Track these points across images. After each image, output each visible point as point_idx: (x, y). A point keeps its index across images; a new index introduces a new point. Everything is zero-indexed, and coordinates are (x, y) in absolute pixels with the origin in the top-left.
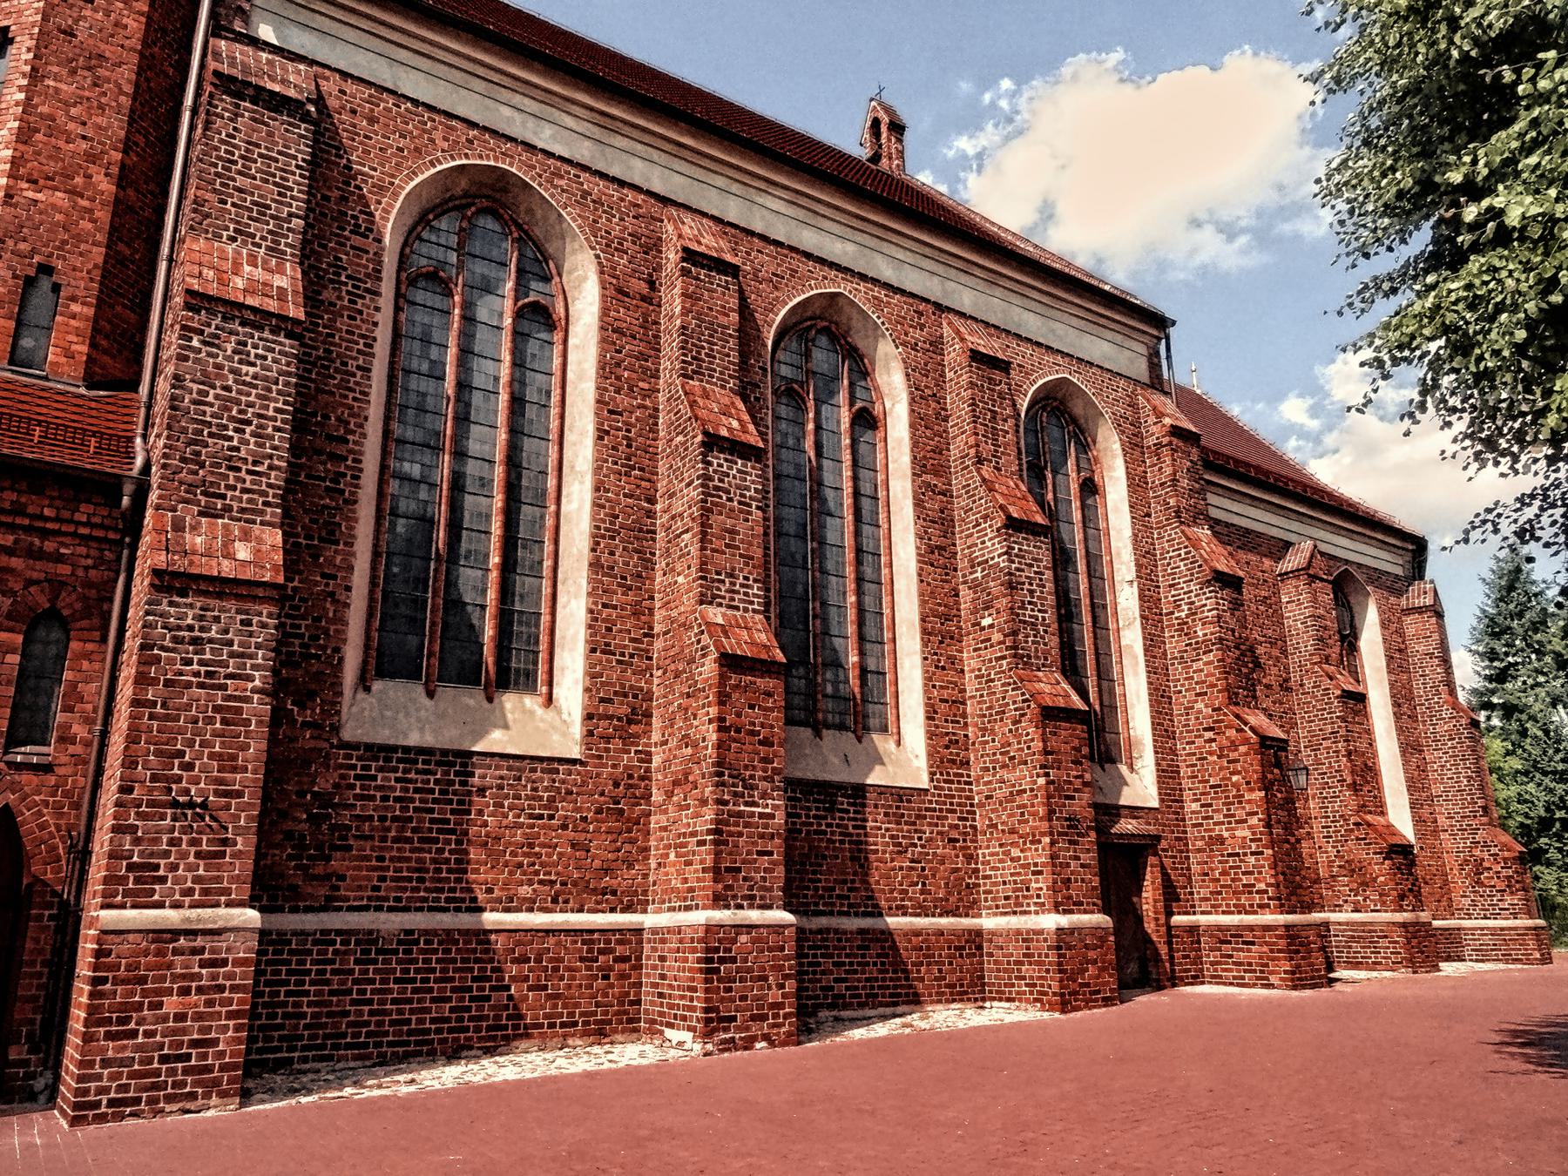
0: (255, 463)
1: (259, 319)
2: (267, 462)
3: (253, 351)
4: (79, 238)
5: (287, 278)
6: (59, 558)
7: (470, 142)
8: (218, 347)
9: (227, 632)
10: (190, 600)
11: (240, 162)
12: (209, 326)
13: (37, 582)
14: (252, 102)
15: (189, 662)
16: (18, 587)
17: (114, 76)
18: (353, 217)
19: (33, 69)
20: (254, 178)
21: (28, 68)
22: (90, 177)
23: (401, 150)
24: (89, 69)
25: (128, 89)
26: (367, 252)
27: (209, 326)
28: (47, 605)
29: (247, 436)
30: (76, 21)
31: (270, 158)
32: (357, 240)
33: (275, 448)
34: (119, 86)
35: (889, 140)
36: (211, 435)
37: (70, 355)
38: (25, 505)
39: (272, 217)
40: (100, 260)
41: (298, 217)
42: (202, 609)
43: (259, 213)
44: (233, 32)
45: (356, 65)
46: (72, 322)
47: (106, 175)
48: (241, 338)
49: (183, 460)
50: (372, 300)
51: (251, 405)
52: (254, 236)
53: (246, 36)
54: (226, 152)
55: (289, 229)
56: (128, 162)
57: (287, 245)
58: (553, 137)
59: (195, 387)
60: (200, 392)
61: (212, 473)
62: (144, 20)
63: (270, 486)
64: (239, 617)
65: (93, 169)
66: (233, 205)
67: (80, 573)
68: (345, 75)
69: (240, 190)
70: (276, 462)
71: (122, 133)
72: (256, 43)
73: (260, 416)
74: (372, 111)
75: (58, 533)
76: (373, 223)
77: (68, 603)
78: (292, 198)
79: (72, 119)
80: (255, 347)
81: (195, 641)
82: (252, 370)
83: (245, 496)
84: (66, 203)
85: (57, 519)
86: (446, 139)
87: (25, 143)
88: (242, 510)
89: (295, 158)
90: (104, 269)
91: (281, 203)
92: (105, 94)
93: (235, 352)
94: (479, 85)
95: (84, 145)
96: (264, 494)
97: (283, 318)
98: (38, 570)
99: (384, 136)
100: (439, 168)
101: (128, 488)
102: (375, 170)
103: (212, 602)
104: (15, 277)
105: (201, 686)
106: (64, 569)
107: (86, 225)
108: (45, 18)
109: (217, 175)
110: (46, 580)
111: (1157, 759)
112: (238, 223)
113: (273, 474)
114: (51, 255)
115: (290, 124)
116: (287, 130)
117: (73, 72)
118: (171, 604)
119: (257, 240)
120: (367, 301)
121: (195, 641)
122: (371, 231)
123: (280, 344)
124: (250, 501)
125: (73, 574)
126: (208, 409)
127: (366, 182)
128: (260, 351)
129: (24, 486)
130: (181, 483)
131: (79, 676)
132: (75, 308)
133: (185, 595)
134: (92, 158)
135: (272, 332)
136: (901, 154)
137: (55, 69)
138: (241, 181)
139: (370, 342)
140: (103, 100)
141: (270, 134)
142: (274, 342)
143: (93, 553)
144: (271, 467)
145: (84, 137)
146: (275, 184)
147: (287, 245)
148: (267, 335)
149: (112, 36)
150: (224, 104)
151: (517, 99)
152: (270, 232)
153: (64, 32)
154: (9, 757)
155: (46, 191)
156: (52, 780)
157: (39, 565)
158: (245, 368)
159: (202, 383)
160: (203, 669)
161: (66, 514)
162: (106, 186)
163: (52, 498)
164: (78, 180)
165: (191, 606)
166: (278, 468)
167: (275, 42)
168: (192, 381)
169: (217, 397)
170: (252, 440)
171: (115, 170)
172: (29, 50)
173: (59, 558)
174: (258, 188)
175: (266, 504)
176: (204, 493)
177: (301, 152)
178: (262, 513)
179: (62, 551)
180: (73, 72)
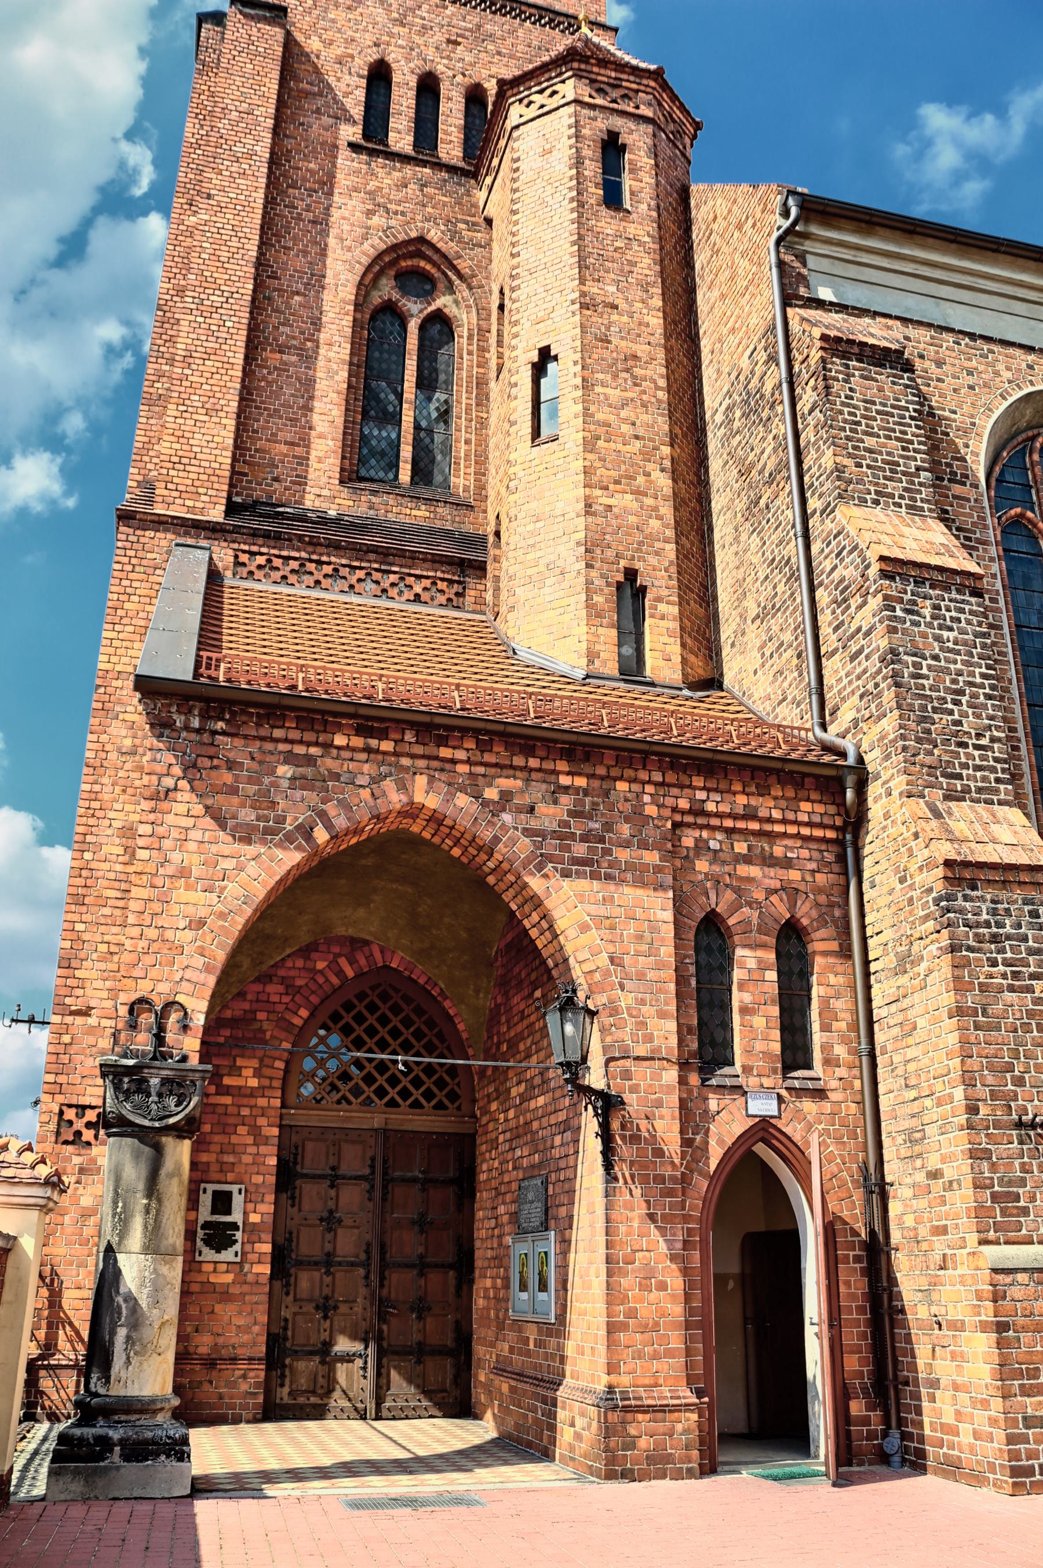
0: (979, 736)
2: (988, 734)
3: (948, 614)
7: (1031, 367)
8: (919, 614)
9: (1019, 926)
10: (979, 893)
11: (863, 422)
12: (906, 592)
13: (776, 891)
14: (858, 360)
15: (994, 963)
16: (760, 896)
17: (649, 373)
18: (948, 465)
19: (584, 380)
20: (879, 436)
21: (578, 381)
22: (648, 475)
23: (971, 388)
24: (627, 370)
25: (662, 383)
26: (968, 500)
27: (906, 592)
28: (788, 916)
29: (965, 707)
30: (608, 329)
31: (887, 414)
32: (957, 489)
33: (991, 718)
34: (654, 382)
36: (935, 710)
38: (756, 809)
39: (904, 474)
40: (672, 556)
41: (925, 470)
42: (993, 902)
43: (892, 471)
44: (802, 298)
45: (908, 309)
46: (662, 623)
47: (662, 470)
48: (934, 601)
49: (919, 740)
50: (985, 550)
51: (959, 673)
52: (892, 496)
53: (809, 299)
54: (850, 414)
55: (921, 484)
56: (676, 455)
57: (922, 500)
59: (910, 659)
60: (915, 665)
61: (946, 751)
62: (661, 315)
63: (997, 760)
64: (1027, 908)
65: (649, 466)
66: (869, 467)
67: (809, 878)
69: (871, 451)
70: (995, 733)
71: (666, 427)
72: (820, 304)
73: (971, 684)
74: (937, 352)
75: (785, 835)
76: (966, 468)
78: (915, 451)
79: (624, 421)
80: (948, 610)
81: (995, 939)
82: (952, 635)
83: (979, 774)
84: (635, 505)
85: (784, 821)
86: (1008, 369)
87: (591, 452)
88: (979, 790)
89: (907, 409)
90: (678, 565)
91: (908, 458)
92: (644, 392)
93: (934, 617)
95: (638, 444)
96: (993, 770)
99: (954, 377)
100: (1011, 400)
101: (850, 780)
102: (955, 412)
103: (1003, 895)
104: (608, 584)
105: (1012, 989)
106: (794, 875)
107: (655, 523)
108: (583, 331)
109: (848, 438)
110: (783, 889)
112: (877, 484)
113: (996, 746)
114: (633, 558)
115: (894, 376)
116: (893, 383)
117: (615, 376)
118: (966, 898)
119: (897, 500)
120: (981, 553)
121: (995, 939)
122: (967, 477)
123: (968, 603)
124: (984, 779)
125: (803, 880)
126: (925, 682)
127: (950, 426)
128: (954, 614)
129: (753, 789)
130: (922, 765)
131: (831, 992)
132: (662, 607)
133: (974, 888)
135: (959, 592)
137: (600, 376)
138: (870, 442)
140: (644, 397)
141: (881, 390)
142: (963, 602)
143: (816, 855)
144: (993, 740)
145: (637, 437)
146: (897, 439)
147: (922, 500)
148: (954, 595)
149: (639, 336)
150: (836, 365)
152: (905, 489)
153: (602, 341)
154: (789, 1083)
155: (616, 495)
156: (827, 1107)
157: (772, 872)
158: (945, 634)
159: (915, 655)
160: (1008, 969)
161: (790, 816)
162: (664, 482)
163: (775, 798)
164: (641, 479)
165: (982, 899)
166: (998, 740)
167: (835, 300)
168: (906, 653)
169: (930, 668)
170: (970, 711)
171: (667, 463)
172: (575, 363)
173: (787, 863)
174: (884, 446)
175: (998, 780)
176: (945, 775)
178: (997, 791)
179: (789, 855)
180: (615, 376)
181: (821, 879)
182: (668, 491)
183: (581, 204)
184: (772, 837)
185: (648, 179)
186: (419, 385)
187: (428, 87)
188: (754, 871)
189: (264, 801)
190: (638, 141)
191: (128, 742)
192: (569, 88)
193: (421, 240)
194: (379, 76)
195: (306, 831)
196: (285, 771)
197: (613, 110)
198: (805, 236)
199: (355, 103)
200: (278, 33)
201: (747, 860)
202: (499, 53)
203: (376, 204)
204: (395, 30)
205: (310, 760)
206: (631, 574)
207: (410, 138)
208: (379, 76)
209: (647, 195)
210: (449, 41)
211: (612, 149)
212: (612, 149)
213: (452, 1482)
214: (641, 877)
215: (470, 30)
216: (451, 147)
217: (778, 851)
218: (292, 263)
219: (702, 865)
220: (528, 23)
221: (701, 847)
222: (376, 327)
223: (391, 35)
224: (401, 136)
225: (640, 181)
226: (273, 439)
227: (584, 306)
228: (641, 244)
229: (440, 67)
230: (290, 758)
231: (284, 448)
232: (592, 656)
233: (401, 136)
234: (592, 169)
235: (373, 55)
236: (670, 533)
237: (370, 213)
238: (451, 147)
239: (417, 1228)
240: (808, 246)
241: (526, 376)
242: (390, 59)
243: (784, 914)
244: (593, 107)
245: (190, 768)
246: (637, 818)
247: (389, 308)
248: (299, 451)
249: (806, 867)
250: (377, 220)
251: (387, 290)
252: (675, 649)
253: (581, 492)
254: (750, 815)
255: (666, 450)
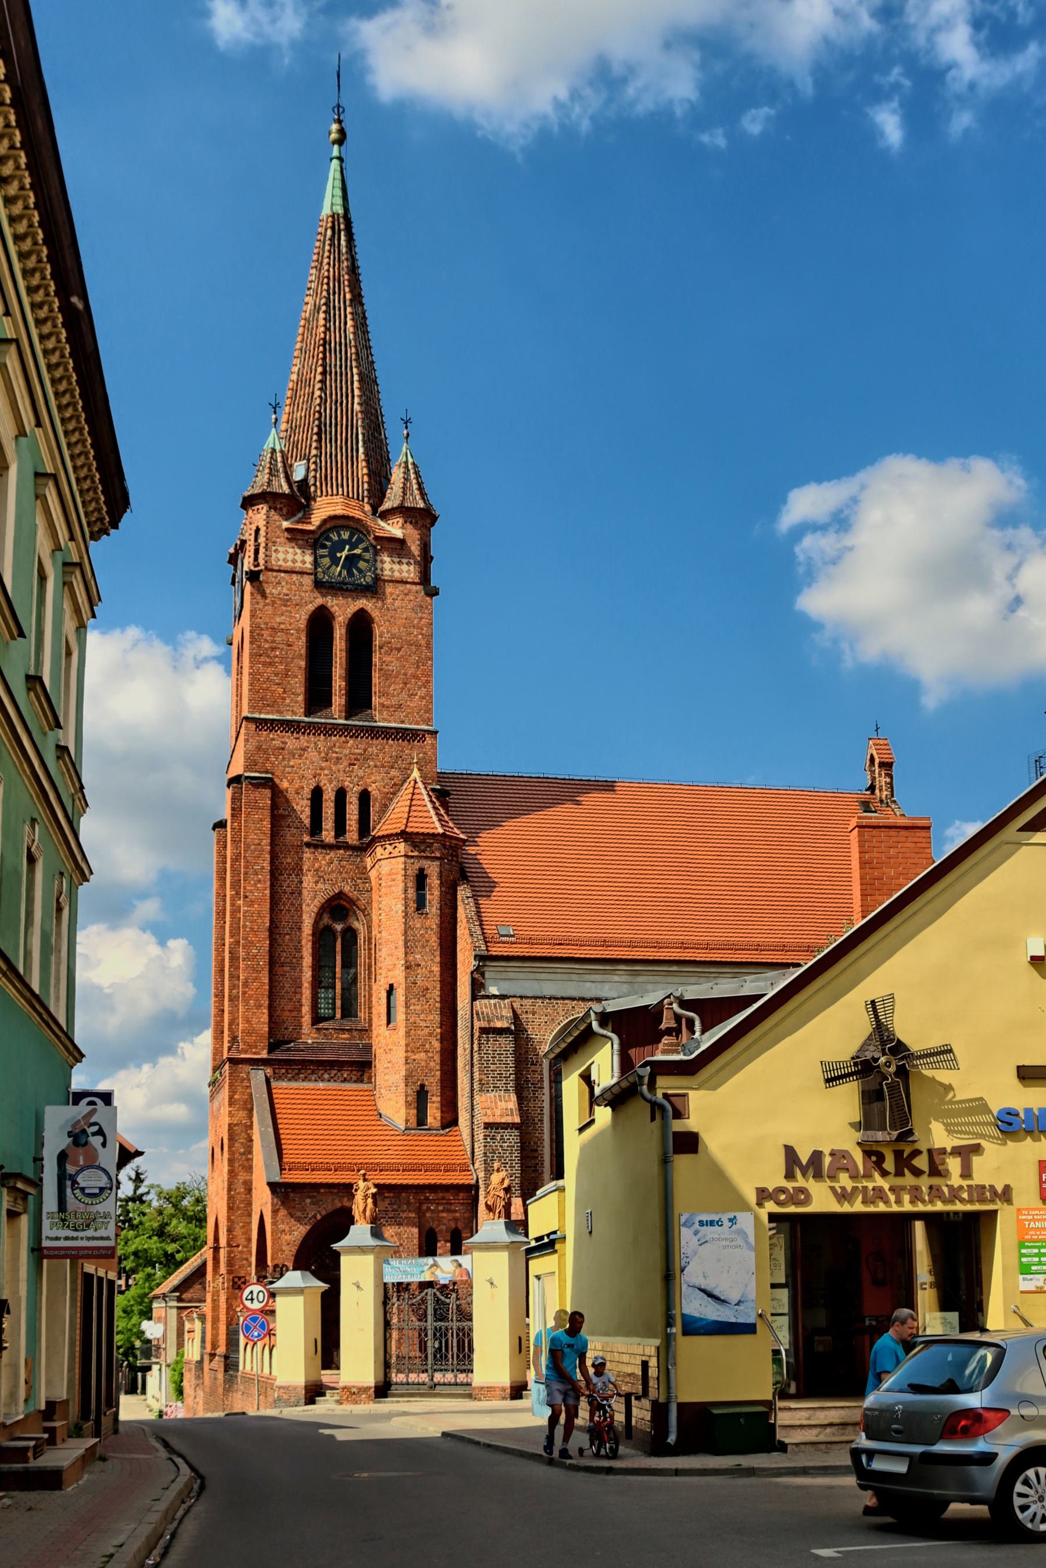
1: (505, 1126)
4: (431, 1070)
5: (511, 1102)
6: (456, 1211)
25: (438, 999)
32: (533, 1068)
35: (880, 775)
37: (435, 1118)
58: (610, 990)
68: (521, 997)
77: (460, 1225)
94: (574, 977)
97: (513, 1124)
98: (451, 1216)
106: (458, 1215)
107: (432, 1064)
111: (471, 1365)
134: (430, 1035)
136: (891, 785)
139: (542, 1108)
151: (593, 977)
162: (437, 1045)
164: (427, 1046)
171: (439, 1037)
173: (456, 1211)
177: (511, 1047)
181: (466, 1215)
182: (438, 1049)
183: (406, 915)
184: (451, 1204)
185: (437, 893)
186: (343, 966)
187: (341, 795)
188: (444, 1215)
189: (303, 1210)
190: (433, 869)
191: (242, 1150)
192: (402, 847)
193: (341, 893)
194: (317, 794)
195: (315, 1216)
196: (308, 1201)
197: (421, 857)
198: (484, 966)
199: (305, 814)
200: (267, 792)
201: (442, 1211)
202: (376, 766)
203: (319, 878)
204: (323, 765)
205: (314, 1197)
206: (422, 1086)
207: (333, 833)
208: (317, 794)
209: (436, 903)
210: (350, 764)
211: (421, 879)
212: (421, 879)
213: (444, 1404)
214: (410, 1223)
215: (361, 754)
216: (352, 836)
217: (453, 1208)
218: (285, 918)
219: (428, 1215)
220: (390, 741)
221: (429, 1208)
222: (322, 936)
223: (322, 769)
224: (328, 835)
225: (433, 895)
226: (283, 1010)
227: (407, 968)
228: (432, 929)
229: (347, 783)
230: (309, 1197)
231: (288, 1014)
232: (407, 1121)
233: (328, 835)
234: (412, 893)
235: (313, 784)
236: (438, 1067)
237: (317, 882)
238: (352, 836)
239: (617, 70)
240: (486, 969)
241: (384, 995)
242: (322, 784)
243: (454, 1226)
244: (412, 857)
245: (283, 1203)
246: (408, 1204)
247: (328, 929)
248: (294, 1014)
249: (460, 1210)
250: (320, 886)
251: (326, 920)
252: (438, 1115)
253: (404, 1055)
254: (443, 1198)
255: (439, 1030)
